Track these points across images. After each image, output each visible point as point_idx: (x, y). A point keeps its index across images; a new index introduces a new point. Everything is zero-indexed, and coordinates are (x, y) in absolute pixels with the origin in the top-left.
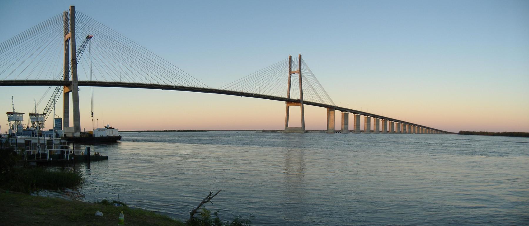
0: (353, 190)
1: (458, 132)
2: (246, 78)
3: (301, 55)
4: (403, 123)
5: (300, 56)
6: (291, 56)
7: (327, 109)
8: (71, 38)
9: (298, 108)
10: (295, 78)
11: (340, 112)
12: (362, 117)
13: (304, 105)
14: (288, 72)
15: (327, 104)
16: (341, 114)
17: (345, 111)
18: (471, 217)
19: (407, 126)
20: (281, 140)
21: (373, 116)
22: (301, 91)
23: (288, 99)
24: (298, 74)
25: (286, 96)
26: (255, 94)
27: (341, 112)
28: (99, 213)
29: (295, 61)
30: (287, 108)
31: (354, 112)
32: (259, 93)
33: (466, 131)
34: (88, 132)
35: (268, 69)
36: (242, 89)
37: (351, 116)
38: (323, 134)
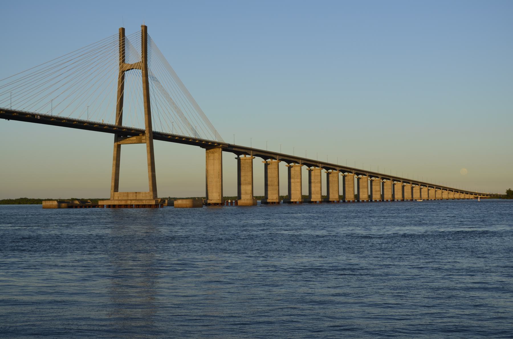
1: (504, 193)
3: (146, 27)
5: (144, 28)
6: (123, 30)
9: (142, 148)
11: (234, 156)
13: (154, 140)
14: (118, 67)
19: (388, 183)
20: (110, 226)
22: (147, 109)
23: (119, 128)
24: (140, 71)
25: (112, 121)
26: (41, 116)
30: (116, 149)
32: (49, 114)
33: (16, 199)
34: (143, 88)
35: (106, 45)
36: (9, 102)
38: (216, 207)
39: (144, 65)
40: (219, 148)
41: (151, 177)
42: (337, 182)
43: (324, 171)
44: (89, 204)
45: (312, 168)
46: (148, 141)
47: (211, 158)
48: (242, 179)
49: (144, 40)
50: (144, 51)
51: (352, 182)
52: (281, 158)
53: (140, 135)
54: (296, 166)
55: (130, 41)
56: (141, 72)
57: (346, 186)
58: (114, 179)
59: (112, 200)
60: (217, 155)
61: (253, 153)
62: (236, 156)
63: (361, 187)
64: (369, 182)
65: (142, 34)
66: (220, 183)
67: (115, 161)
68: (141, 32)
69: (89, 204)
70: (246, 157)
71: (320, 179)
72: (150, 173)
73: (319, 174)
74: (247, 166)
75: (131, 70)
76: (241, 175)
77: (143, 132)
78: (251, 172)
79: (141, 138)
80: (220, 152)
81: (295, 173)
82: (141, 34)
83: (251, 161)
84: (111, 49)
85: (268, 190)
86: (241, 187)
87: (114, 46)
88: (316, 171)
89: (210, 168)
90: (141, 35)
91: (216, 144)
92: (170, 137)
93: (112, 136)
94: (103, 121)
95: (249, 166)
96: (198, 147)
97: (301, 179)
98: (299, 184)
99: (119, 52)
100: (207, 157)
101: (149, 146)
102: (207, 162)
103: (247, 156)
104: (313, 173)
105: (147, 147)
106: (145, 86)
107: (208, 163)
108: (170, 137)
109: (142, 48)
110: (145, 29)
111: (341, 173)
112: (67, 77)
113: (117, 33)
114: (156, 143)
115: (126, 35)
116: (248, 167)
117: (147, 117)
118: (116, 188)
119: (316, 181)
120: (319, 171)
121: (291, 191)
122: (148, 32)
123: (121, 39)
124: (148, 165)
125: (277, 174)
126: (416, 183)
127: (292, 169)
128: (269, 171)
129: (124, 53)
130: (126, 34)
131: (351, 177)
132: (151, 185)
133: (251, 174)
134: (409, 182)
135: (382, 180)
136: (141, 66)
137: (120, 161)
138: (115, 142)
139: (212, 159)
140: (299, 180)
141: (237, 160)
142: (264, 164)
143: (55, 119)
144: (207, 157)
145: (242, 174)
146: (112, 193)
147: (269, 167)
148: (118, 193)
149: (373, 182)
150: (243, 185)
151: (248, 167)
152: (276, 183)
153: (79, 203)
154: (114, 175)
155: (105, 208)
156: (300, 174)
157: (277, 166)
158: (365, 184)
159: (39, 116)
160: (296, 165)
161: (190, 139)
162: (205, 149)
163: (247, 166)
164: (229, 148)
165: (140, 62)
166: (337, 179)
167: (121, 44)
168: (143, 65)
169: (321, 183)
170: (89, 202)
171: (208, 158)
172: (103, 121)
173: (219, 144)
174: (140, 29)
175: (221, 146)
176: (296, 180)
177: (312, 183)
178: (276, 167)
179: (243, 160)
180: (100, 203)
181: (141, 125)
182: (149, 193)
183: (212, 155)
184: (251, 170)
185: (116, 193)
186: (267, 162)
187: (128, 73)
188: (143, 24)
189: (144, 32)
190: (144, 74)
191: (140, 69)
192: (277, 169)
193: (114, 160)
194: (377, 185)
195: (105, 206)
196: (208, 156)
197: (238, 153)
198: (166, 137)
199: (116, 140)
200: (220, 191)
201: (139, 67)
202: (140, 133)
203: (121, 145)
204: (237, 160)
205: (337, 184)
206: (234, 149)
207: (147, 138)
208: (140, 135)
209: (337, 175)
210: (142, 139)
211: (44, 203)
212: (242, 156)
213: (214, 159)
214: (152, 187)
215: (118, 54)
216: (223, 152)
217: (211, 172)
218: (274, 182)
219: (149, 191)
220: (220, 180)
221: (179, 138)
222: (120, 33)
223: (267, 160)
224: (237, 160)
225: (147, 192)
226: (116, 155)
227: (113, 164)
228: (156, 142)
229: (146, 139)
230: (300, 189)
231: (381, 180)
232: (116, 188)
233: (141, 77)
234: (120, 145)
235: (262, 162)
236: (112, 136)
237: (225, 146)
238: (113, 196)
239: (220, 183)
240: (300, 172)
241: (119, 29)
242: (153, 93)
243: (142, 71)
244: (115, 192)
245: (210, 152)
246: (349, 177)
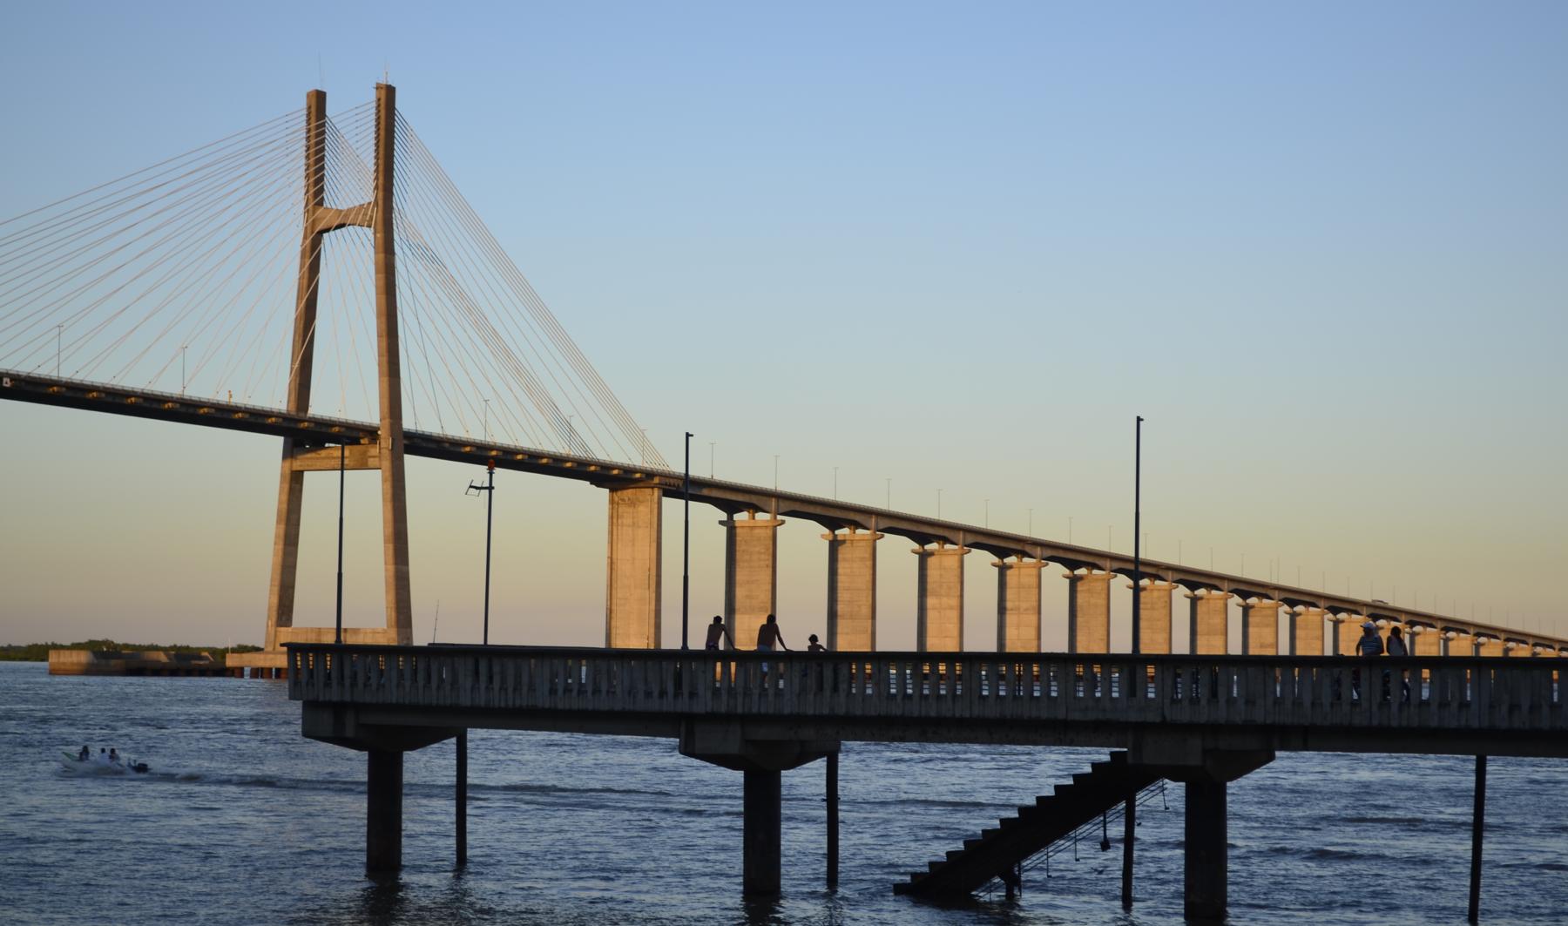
5: (383, 92)
11: (908, 544)
24: (370, 232)
25: (275, 397)
26: (15, 378)
39: (380, 213)
40: (653, 488)
41: (392, 580)
42: (1104, 610)
43: (1182, 591)
44: (202, 663)
45: (1201, 592)
46: (387, 464)
47: (625, 521)
48: (740, 592)
49: (382, 133)
50: (381, 168)
51: (1165, 611)
52: (971, 539)
53: (362, 441)
54: (946, 553)
55: (342, 132)
56: (371, 237)
57: (1143, 624)
58: (277, 583)
59: (268, 653)
60: (644, 511)
61: (964, 539)
62: (723, 516)
63: (1200, 628)
64: (1329, 626)
65: (378, 111)
66: (653, 607)
67: (282, 527)
68: (374, 104)
69: (202, 663)
70: (754, 518)
71: (1035, 598)
72: (391, 568)
73: (1034, 581)
74: (757, 549)
75: (332, 233)
76: (735, 580)
77: (371, 433)
78: (771, 569)
79: (365, 453)
80: (656, 500)
81: (941, 575)
82: (374, 111)
83: (770, 532)
84: (277, 166)
85: (836, 634)
86: (734, 619)
87: (289, 158)
88: (1023, 571)
89: (623, 553)
90: (374, 117)
91: (638, 475)
92: (468, 449)
93: (277, 442)
94: (231, 396)
95: (763, 551)
96: (584, 485)
97: (962, 596)
98: (955, 614)
99: (304, 174)
100: (612, 517)
101: (390, 478)
102: (611, 533)
103: (860, 531)
104: (1011, 575)
105: (384, 481)
106: (382, 283)
107: (615, 537)
108: (468, 449)
109: (377, 158)
110: (388, 96)
111: (1237, 599)
112: (121, 248)
113: (301, 105)
114: (414, 465)
115: (328, 113)
116: (760, 553)
117: (386, 385)
118: (284, 611)
119: (1024, 605)
120: (1034, 571)
121: (926, 637)
122: (398, 105)
123: (313, 125)
124: (385, 542)
125: (869, 577)
126: (1547, 643)
127: (931, 561)
128: (842, 568)
129: (321, 179)
130: (330, 110)
131: (1162, 593)
132: (393, 605)
133: (769, 579)
134: (1465, 628)
135: (1411, 628)
136: (371, 217)
137: (298, 524)
138: (285, 457)
139: (629, 526)
140: (955, 602)
141: (725, 528)
142: (827, 543)
143: (103, 395)
144: (614, 518)
145: (741, 575)
146: (272, 630)
147: (843, 552)
148: (290, 629)
149: (1199, 603)
150: (743, 613)
151: (760, 553)
152: (866, 610)
153: (170, 659)
154: (278, 571)
155: (247, 678)
156: (957, 580)
157: (869, 550)
158: (1217, 620)
159: (8, 380)
160: (947, 550)
161: (568, 461)
162: (608, 490)
163: (757, 549)
164: (687, 488)
165: (370, 203)
166: (1103, 602)
167: (312, 150)
168: (378, 215)
169: (1039, 613)
170: (206, 658)
171: (615, 521)
172: (231, 396)
173: (650, 475)
174: (371, 96)
175: (656, 480)
176: (945, 600)
177: (1008, 612)
178: (868, 555)
179: (745, 530)
180: (231, 661)
181: (365, 409)
182: (385, 632)
183: (631, 510)
184: (770, 563)
185: (283, 629)
186: (835, 536)
187: (333, 238)
188: (383, 81)
189: (383, 106)
190: (381, 242)
191: (369, 226)
192: (869, 563)
193: (278, 522)
194: (1267, 626)
195: (247, 671)
196: (615, 515)
197: (730, 507)
198: (458, 449)
199: (289, 453)
200: (652, 630)
201: (363, 220)
202: (361, 434)
203: (305, 473)
204: (724, 529)
205: (1103, 619)
206: (705, 492)
207: (382, 451)
208: (362, 441)
209: (1105, 586)
210: (369, 454)
211: (53, 657)
212: (741, 517)
213: (634, 523)
214: (393, 614)
215: (303, 182)
216: (664, 499)
217: (623, 568)
218: (859, 606)
219: (385, 628)
220: (653, 595)
221: (598, 469)
222: (309, 108)
223: (837, 532)
224: (917, 556)
225: (380, 630)
226: (285, 506)
227: (277, 536)
228: (411, 461)
229: (380, 456)
230: (955, 633)
231: (1442, 636)
232: (284, 611)
233: (372, 251)
234: (302, 472)
235: (823, 536)
236: (277, 442)
237: (672, 481)
238: (272, 638)
239: (653, 603)
240: (957, 572)
241: (308, 95)
242: (411, 303)
243: (375, 233)
244: (281, 626)
245: (623, 500)
246: (1156, 594)
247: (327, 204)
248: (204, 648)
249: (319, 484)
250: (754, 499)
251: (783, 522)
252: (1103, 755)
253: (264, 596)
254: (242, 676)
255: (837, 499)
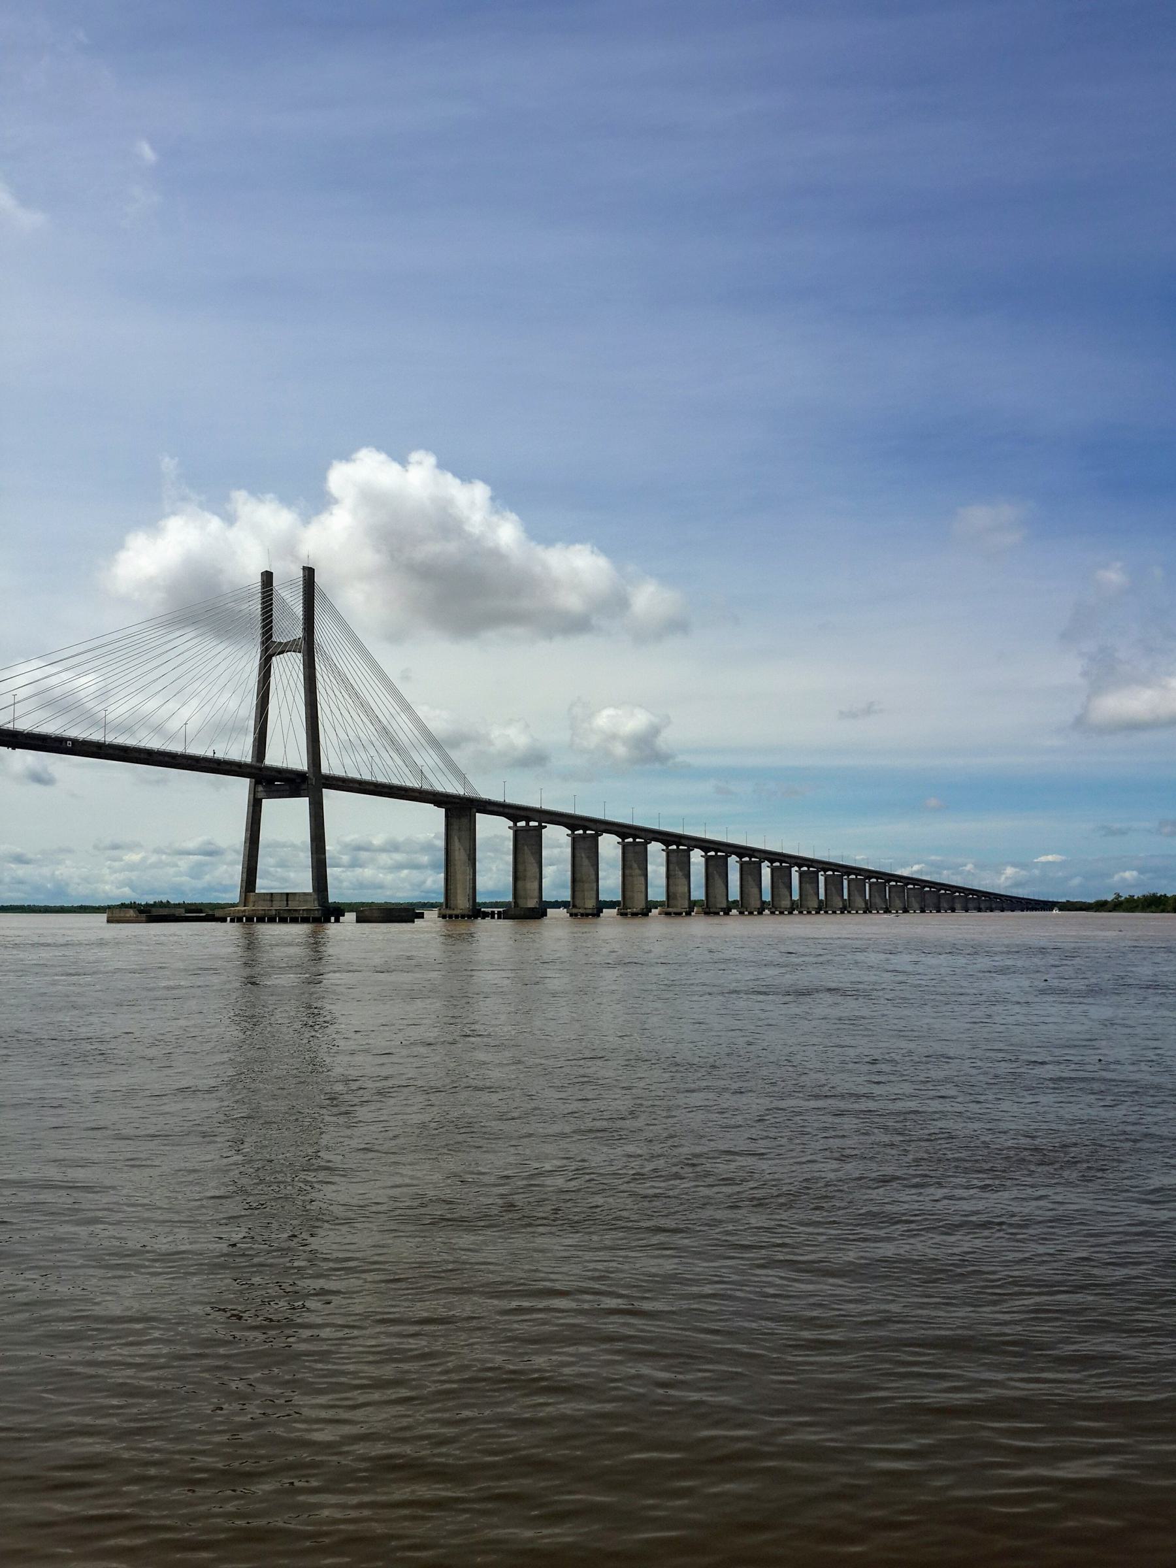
0: (451, 1142)
2: (128, 631)
4: (713, 850)
7: (249, 779)
8: (122, 863)
10: (288, 668)
12: (655, 848)
15: (439, 788)
16: (738, 864)
17: (635, 837)
18: (1064, 1075)
21: (697, 843)
24: (300, 655)
25: (241, 750)
27: (511, 824)
28: (147, 152)
29: (290, 599)
31: (666, 838)
37: (655, 850)
130: (276, 582)
181: (298, 761)
191: (300, 652)
247: (274, 639)
248: (350, 904)
249: (270, 806)
250: (529, 814)
251: (546, 827)
252: (1064, 858)
253: (235, 873)
254: (301, 918)
255: (576, 813)
